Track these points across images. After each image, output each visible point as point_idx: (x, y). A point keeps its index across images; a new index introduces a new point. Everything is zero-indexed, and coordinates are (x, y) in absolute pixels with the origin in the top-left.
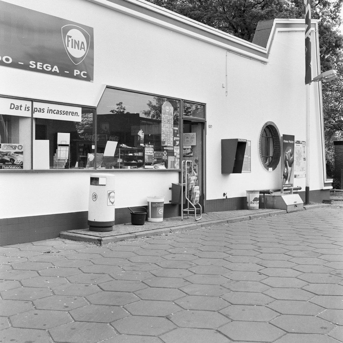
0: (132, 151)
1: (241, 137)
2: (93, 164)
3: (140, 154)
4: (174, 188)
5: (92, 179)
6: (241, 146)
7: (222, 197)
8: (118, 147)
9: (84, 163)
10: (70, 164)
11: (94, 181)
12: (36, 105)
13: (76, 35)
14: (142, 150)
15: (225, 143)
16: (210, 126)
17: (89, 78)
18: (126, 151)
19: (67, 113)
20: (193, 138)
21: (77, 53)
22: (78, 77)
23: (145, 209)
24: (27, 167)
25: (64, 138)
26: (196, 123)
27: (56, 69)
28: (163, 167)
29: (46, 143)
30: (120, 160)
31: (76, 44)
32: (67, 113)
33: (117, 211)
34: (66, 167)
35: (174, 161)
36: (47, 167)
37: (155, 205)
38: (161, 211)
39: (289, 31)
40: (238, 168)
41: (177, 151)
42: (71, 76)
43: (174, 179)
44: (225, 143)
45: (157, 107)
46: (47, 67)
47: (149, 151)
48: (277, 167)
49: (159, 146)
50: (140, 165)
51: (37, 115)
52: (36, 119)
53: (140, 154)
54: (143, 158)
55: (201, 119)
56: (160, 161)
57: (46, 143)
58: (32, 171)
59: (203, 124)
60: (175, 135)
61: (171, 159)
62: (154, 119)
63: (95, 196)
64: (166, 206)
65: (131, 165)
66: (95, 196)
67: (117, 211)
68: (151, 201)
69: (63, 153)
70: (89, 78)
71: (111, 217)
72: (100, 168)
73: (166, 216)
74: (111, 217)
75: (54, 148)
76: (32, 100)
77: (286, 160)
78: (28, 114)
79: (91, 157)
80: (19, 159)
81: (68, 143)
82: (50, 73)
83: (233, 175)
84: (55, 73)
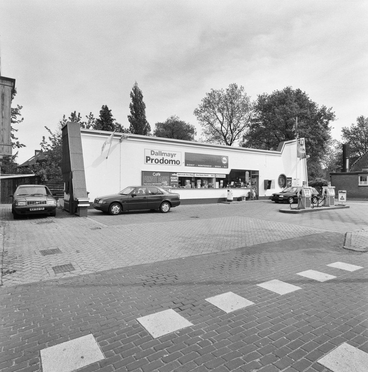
0: (237, 184)
1: (269, 179)
2: (228, 187)
3: (240, 184)
4: (249, 193)
5: (228, 190)
6: (270, 182)
7: (264, 196)
8: (234, 183)
9: (226, 187)
10: (223, 187)
11: (228, 191)
12: (216, 175)
13: (224, 159)
14: (240, 183)
15: (265, 181)
16: (260, 176)
17: (227, 168)
18: (236, 184)
19: (222, 176)
20: (255, 180)
21: (224, 163)
22: (225, 168)
23: (241, 198)
24: (214, 188)
25: (222, 181)
26: (256, 176)
27: (220, 167)
28: (246, 188)
29: (218, 183)
30: (235, 186)
31: (224, 161)
32: (222, 176)
33: (233, 198)
34: (222, 188)
35: (249, 186)
36: (218, 188)
37: (243, 197)
38: (245, 198)
39: (275, 155)
40: (269, 187)
41: (250, 183)
42: (223, 168)
43: (249, 191)
44: (265, 181)
45: (351, 149)
46: (218, 166)
47: (242, 184)
48: (129, 121)
49: (245, 183)
50: (239, 187)
51: (216, 177)
52: (216, 178)
53: (240, 184)
54: (240, 185)
55: (257, 175)
56: (245, 186)
57: (218, 183)
58: (215, 189)
59: (258, 176)
60: (249, 179)
61: (248, 186)
62: (13, 365)
63: (229, 194)
64: (246, 198)
65: (237, 187)
66: (229, 194)
67: (233, 198)
68: (242, 196)
69: (222, 185)
70: (227, 168)
71: (232, 199)
72: (230, 188)
73: (246, 200)
74: (232, 199)
75: (220, 184)
76: (215, 174)
77: (288, 185)
78: (215, 177)
79: (228, 185)
80: (213, 186)
81: (223, 182)
82: (219, 168)
83: (268, 190)
84: (220, 168)
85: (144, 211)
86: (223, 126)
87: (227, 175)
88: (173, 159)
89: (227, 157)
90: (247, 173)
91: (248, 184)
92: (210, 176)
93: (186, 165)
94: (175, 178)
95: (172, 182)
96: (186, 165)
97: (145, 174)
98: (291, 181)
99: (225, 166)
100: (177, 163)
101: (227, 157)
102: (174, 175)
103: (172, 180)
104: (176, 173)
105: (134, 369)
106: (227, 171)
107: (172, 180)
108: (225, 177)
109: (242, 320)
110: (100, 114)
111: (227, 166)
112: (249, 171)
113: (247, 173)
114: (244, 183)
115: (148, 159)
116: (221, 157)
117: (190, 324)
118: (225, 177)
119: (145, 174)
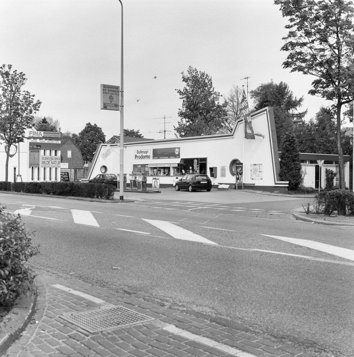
17: (179, 157)
22: (178, 158)
42: (176, 158)
46: (173, 157)
47: (191, 171)
85: (293, 252)
86: (237, 101)
87: (178, 164)
88: (146, 155)
89: (179, 148)
90: (196, 161)
91: (196, 172)
92: (167, 166)
93: (153, 159)
94: (147, 168)
95: (146, 171)
96: (153, 159)
97: (135, 166)
98: (242, 167)
99: (178, 156)
100: (148, 157)
101: (179, 148)
102: (147, 166)
103: (146, 170)
104: (148, 165)
105: (131, 335)
106: (177, 161)
107: (146, 170)
108: (177, 166)
109: (184, 350)
110: (253, 90)
111: (179, 155)
112: (197, 159)
113: (196, 161)
114: (192, 171)
115: (136, 156)
116: (174, 149)
117: (99, 226)
118: (177, 166)
119: (135, 166)
